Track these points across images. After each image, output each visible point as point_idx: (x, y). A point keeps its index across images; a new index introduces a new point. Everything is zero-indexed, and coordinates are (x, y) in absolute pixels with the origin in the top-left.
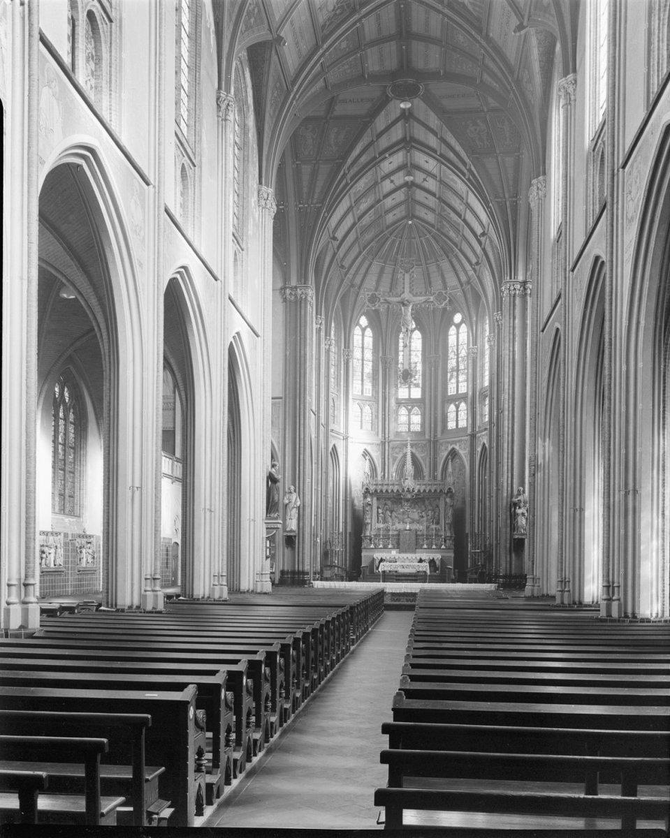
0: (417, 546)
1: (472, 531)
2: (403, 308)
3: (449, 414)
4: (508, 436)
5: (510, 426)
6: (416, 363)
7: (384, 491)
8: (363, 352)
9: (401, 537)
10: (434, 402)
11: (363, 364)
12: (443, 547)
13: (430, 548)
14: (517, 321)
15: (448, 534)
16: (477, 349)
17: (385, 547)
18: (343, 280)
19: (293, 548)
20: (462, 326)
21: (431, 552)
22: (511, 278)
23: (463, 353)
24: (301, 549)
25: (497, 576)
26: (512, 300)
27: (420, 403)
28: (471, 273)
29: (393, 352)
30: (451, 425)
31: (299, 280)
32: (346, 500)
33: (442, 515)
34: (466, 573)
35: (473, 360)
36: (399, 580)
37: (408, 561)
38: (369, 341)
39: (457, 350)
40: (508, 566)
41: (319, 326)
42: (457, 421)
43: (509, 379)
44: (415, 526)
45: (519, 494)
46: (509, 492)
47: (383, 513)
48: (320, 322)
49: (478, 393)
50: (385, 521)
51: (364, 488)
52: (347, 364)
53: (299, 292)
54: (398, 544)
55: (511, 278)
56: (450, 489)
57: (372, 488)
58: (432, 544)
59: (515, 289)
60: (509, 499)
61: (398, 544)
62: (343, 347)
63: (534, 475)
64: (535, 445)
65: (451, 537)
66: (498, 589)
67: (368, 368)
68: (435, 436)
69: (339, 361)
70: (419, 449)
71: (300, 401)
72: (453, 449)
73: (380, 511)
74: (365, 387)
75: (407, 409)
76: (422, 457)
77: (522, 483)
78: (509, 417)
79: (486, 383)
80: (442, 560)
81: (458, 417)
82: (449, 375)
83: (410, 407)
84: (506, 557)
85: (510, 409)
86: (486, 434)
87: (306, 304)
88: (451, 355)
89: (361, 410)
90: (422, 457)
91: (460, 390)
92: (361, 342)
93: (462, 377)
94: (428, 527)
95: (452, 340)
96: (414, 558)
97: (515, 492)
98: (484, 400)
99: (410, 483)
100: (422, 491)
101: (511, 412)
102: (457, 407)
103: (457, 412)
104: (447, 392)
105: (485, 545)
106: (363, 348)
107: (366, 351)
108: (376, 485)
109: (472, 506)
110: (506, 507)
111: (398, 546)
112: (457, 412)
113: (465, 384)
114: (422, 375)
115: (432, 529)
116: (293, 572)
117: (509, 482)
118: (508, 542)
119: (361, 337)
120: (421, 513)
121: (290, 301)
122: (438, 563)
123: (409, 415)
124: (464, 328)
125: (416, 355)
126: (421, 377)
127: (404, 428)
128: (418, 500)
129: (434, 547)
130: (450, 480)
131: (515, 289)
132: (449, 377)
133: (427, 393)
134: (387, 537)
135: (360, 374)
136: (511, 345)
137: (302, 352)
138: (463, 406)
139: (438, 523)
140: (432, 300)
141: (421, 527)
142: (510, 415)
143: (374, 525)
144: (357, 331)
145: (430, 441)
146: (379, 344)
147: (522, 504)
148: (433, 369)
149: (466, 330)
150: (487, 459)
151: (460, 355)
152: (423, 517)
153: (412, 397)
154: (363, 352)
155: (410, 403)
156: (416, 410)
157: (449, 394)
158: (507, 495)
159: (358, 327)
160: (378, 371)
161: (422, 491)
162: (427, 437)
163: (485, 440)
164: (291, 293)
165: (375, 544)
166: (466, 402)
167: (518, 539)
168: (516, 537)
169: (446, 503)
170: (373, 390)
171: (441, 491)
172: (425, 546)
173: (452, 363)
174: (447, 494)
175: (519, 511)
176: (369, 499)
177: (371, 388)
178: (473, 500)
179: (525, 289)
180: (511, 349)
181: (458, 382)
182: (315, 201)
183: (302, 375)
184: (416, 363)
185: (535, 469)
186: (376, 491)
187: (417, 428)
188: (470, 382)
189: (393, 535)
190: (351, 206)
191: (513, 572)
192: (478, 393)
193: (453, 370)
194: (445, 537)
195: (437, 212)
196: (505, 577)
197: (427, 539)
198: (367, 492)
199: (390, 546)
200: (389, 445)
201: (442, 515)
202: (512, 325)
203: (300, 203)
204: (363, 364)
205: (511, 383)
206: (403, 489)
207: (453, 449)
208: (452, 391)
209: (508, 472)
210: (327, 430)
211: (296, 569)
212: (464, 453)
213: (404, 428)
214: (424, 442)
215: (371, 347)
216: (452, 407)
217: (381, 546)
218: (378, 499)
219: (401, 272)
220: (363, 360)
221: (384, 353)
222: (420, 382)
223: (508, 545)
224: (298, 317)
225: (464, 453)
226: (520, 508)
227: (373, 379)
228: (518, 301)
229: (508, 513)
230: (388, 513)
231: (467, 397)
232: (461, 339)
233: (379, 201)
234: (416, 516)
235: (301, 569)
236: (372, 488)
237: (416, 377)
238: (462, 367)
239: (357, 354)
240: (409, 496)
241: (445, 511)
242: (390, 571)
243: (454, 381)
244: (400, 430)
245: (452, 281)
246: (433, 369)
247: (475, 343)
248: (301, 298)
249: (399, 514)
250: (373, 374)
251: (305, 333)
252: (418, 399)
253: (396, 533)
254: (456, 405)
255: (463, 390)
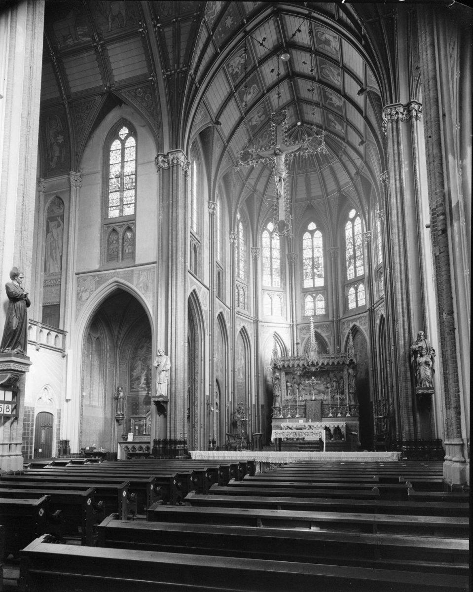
0: (322, 414)
1: (376, 401)
2: (275, 158)
3: (349, 297)
4: (401, 274)
5: (402, 262)
6: (318, 258)
7: (286, 366)
8: (271, 251)
9: (308, 407)
10: (336, 287)
11: (271, 261)
12: (348, 415)
13: (335, 416)
14: (402, 147)
15: (353, 403)
16: (370, 233)
17: (293, 417)
18: (244, 184)
19: (165, 416)
20: (356, 220)
21: (337, 421)
22: (391, 102)
23: (359, 242)
24: (173, 416)
25: (401, 443)
26: (395, 126)
27: (323, 290)
28: (359, 162)
29: (298, 250)
30: (352, 306)
31: (171, 147)
32: (257, 376)
33: (346, 386)
34: (170, 439)
35: (368, 244)
36: (302, 448)
37: (316, 431)
38: (276, 242)
39: (354, 240)
40: (412, 428)
41: (211, 211)
42: (357, 301)
43: (397, 210)
44: (321, 397)
45: (419, 340)
46: (407, 339)
47: (291, 386)
48: (213, 206)
49: (373, 272)
50: (293, 393)
51: (273, 363)
52: (255, 259)
53: (171, 157)
54: (305, 413)
55: (391, 102)
56: (352, 360)
57: (280, 364)
58: (337, 413)
59: (397, 113)
60: (407, 348)
61: (305, 413)
62: (251, 245)
63: (444, 231)
64: (442, 174)
65: (356, 405)
66: (401, 460)
67: (277, 265)
68: (338, 316)
69: (248, 258)
70: (324, 329)
71: (172, 263)
72: (355, 326)
73: (289, 384)
74: (274, 280)
75: (312, 296)
76: (326, 336)
77: (423, 326)
78: (400, 252)
79: (381, 261)
80: (347, 427)
81: (358, 298)
82: (347, 263)
83: (314, 295)
84: (409, 419)
85: (401, 243)
86: (383, 305)
87: (177, 169)
88: (349, 246)
89: (271, 299)
90: (326, 336)
91: (357, 274)
92: (269, 243)
93: (359, 263)
94: (333, 397)
95: (348, 233)
96: (319, 426)
97: (415, 338)
98: (380, 277)
99: (313, 356)
100: (325, 364)
101: (402, 247)
102: (356, 289)
103: (356, 293)
104: (347, 277)
105: (389, 411)
106: (271, 248)
107: (274, 251)
108: (284, 360)
109: (375, 377)
110: (404, 356)
111: (305, 416)
112: (356, 293)
113: (362, 268)
114: (324, 267)
115: (337, 399)
116: (165, 442)
117: (406, 327)
118: (410, 399)
119: (269, 240)
120: (326, 384)
121: (163, 169)
122: (343, 430)
123: (314, 302)
124: (358, 221)
125: (318, 251)
126: (323, 268)
127: (310, 313)
128: (322, 372)
129: (339, 415)
130: (352, 352)
131: (397, 113)
132: (347, 265)
133: (329, 283)
134: (294, 407)
135: (269, 269)
136: (397, 173)
137: (174, 214)
138: (361, 287)
139: (342, 393)
140: (306, 147)
141: (327, 397)
142: (402, 250)
143: (282, 396)
144: (266, 234)
145: (333, 321)
146: (285, 242)
147: (424, 351)
148: (332, 259)
149: (360, 221)
150: (385, 329)
151: (356, 245)
152: (327, 388)
153: (316, 286)
154: (271, 251)
155: (315, 291)
156: (320, 297)
157: (348, 279)
158: (404, 343)
159: (266, 231)
160: (285, 266)
161: (325, 364)
162: (331, 318)
163: (383, 312)
164: (164, 161)
165: (284, 414)
166: (364, 283)
167: (422, 394)
168: (420, 391)
169: (349, 374)
170: (281, 282)
171: (344, 363)
172: (331, 415)
173: (349, 253)
174: (349, 365)
175: (421, 360)
176: (277, 374)
177: (279, 281)
178: (375, 370)
179: (409, 112)
180: (398, 177)
181: (355, 267)
182: (181, 66)
183: (174, 237)
184: (318, 258)
185: (445, 219)
186: (284, 366)
187: (323, 312)
188: (367, 266)
189: (300, 406)
190: (232, 92)
191: (419, 436)
192: (373, 272)
193: (350, 258)
194: (350, 406)
195: (321, 106)
196: (408, 443)
197: (332, 408)
198: (275, 367)
199: (297, 416)
200: (296, 328)
201: (346, 386)
202: (396, 152)
203: (167, 71)
204: (271, 261)
205: (400, 215)
206: (308, 363)
207: (355, 326)
208: (350, 275)
209: (403, 316)
210: (233, 313)
211: (168, 438)
212: (364, 328)
213: (310, 313)
214: (328, 323)
215: (278, 247)
216: (352, 290)
217: (289, 416)
218: (286, 374)
219: (273, 126)
220: (271, 258)
221: (290, 251)
222: (323, 273)
223: (410, 404)
224: (171, 181)
225: (364, 328)
226: (421, 356)
227: (281, 273)
228: (402, 126)
229: (408, 364)
230: (296, 386)
231: (364, 278)
232: (356, 231)
233: (264, 95)
234: (322, 388)
235: (173, 438)
236: (280, 364)
237: (319, 269)
238: (358, 254)
239: (266, 253)
240: (313, 369)
241: (349, 382)
242: (297, 439)
243: (352, 267)
244: (307, 314)
245: (344, 178)
246: (332, 259)
247: (368, 228)
248: (173, 163)
249: (306, 386)
250: (281, 269)
251: (177, 197)
252: (322, 287)
253: (303, 403)
254: (355, 288)
255: (360, 272)
